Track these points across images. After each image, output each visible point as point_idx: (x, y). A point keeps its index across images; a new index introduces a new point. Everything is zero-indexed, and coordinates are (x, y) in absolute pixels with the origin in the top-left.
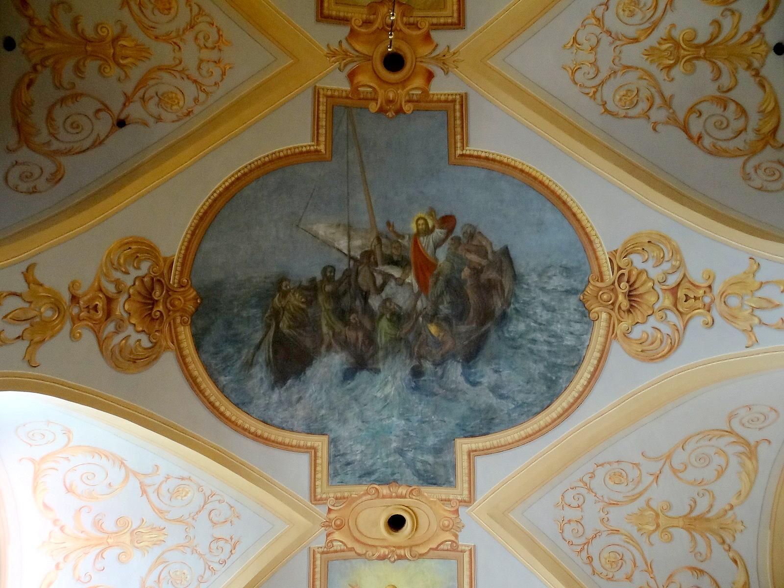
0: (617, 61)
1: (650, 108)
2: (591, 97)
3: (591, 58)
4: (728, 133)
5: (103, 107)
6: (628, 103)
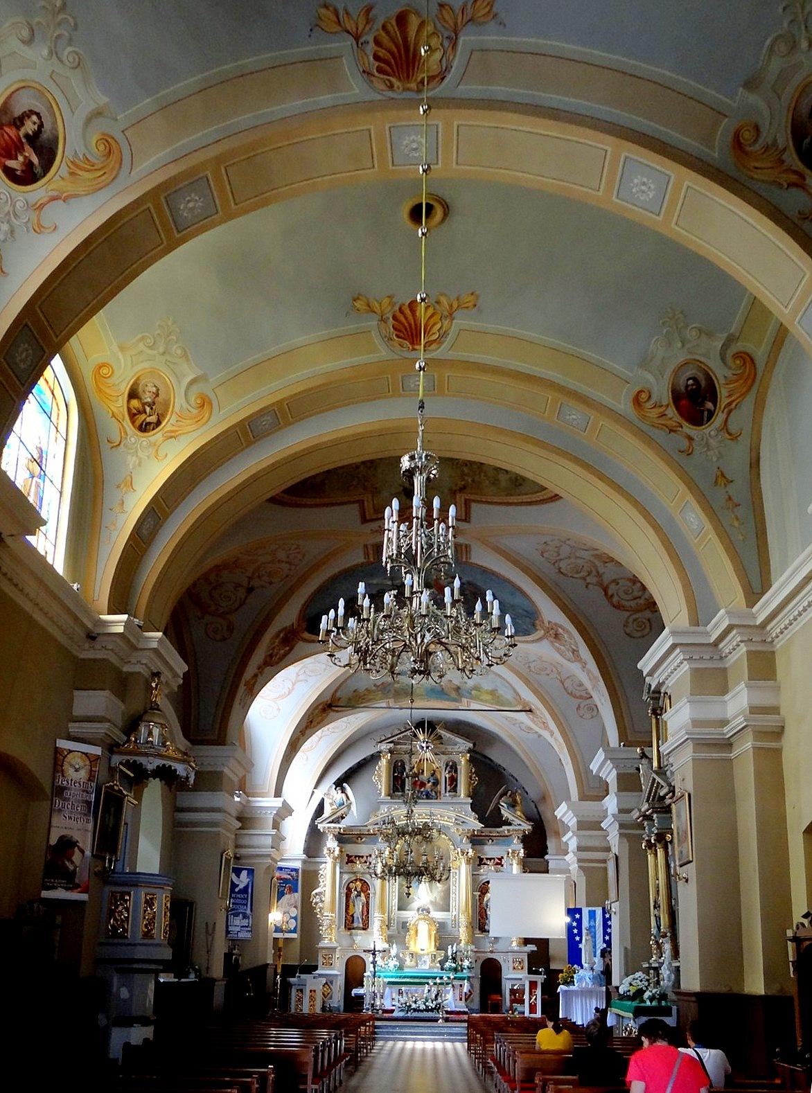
4: (630, 597)
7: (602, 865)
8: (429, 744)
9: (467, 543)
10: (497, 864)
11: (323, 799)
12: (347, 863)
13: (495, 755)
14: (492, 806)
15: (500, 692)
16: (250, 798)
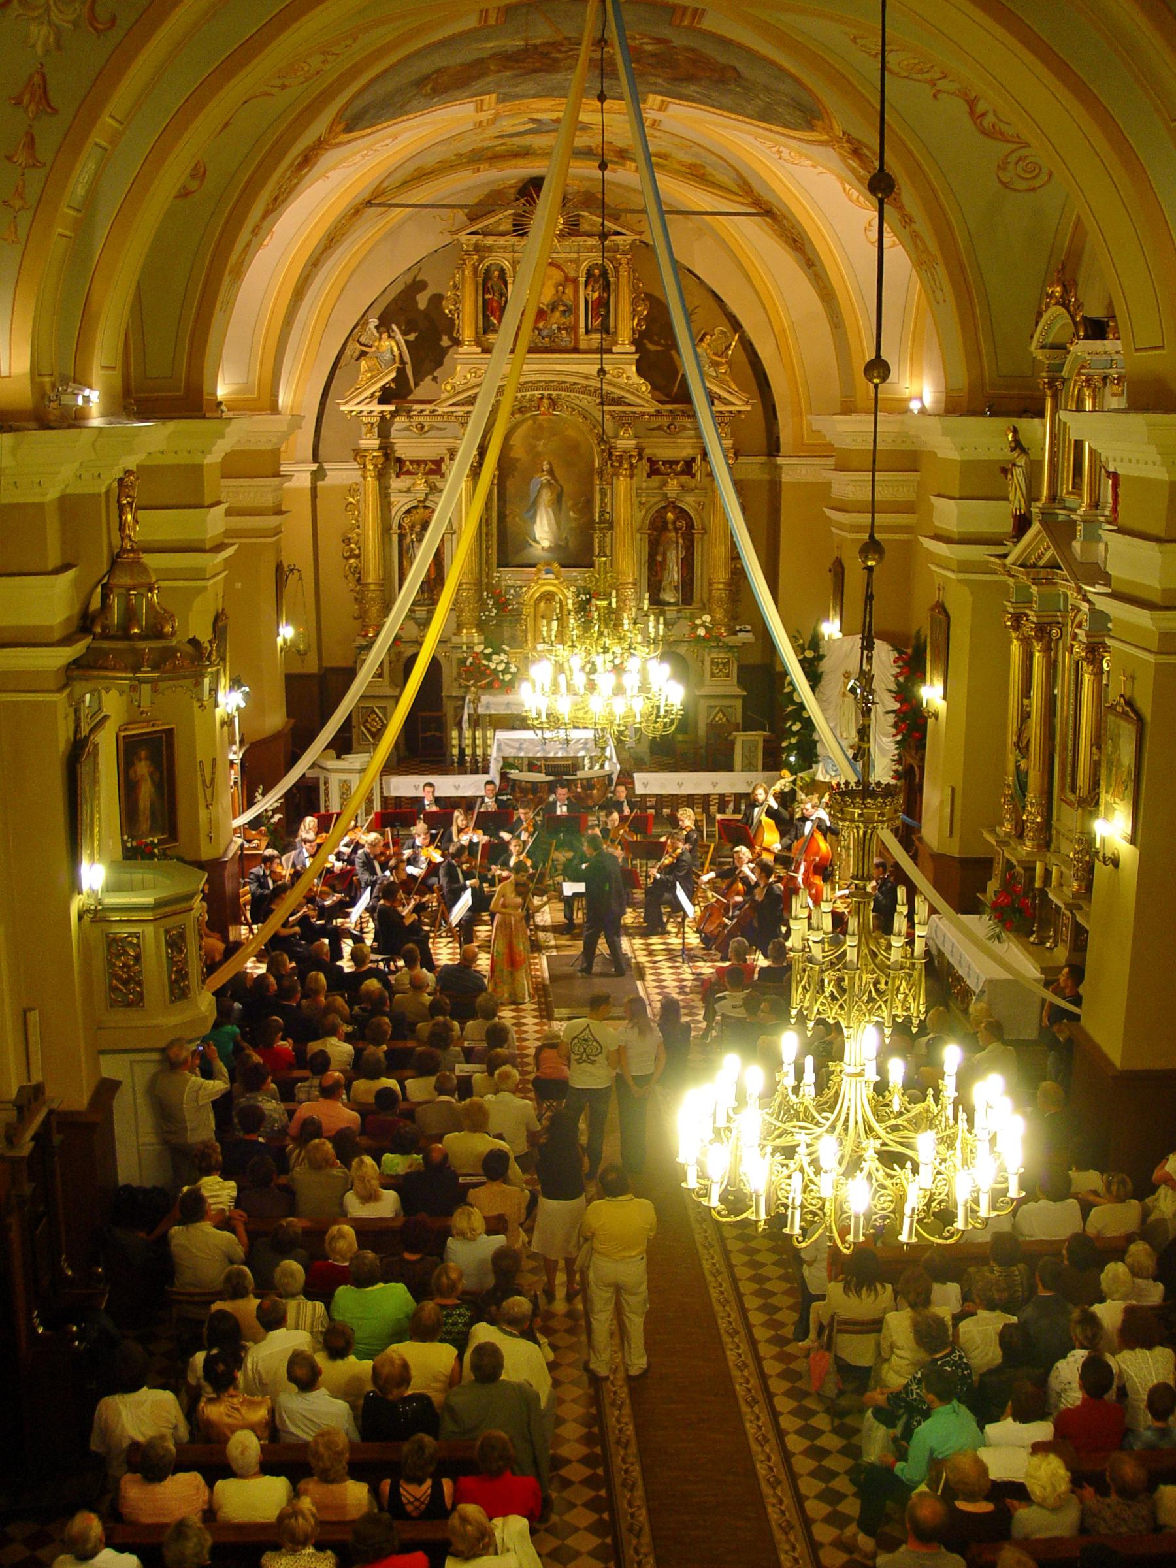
7: (905, 537)
10: (431, 472)
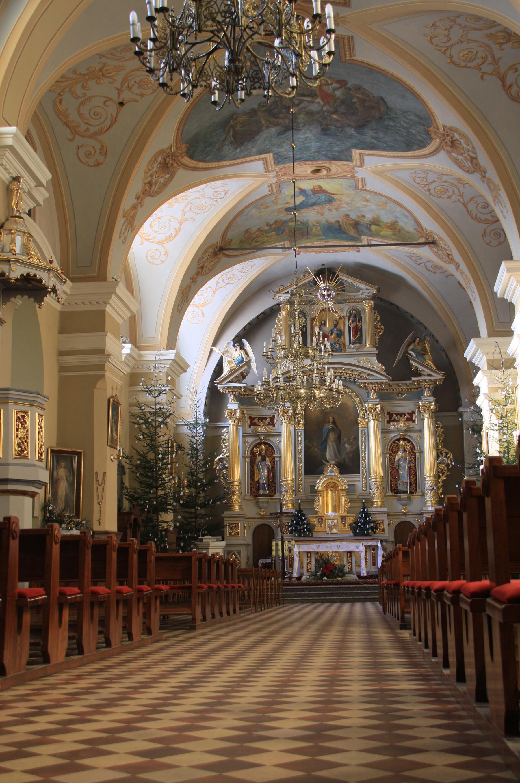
0: (464, 37)
1: (483, 63)
2: (442, 52)
3: (446, 33)
5: (107, 99)
6: (468, 59)
8: (329, 292)
9: (350, 34)
10: (408, 420)
11: (221, 358)
12: (250, 426)
13: (400, 300)
14: (399, 356)
15: (401, 224)
16: (142, 353)
